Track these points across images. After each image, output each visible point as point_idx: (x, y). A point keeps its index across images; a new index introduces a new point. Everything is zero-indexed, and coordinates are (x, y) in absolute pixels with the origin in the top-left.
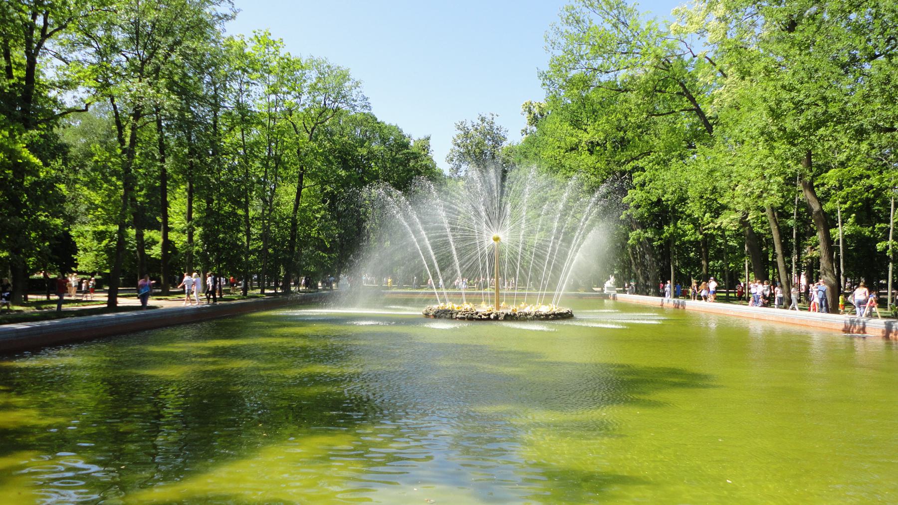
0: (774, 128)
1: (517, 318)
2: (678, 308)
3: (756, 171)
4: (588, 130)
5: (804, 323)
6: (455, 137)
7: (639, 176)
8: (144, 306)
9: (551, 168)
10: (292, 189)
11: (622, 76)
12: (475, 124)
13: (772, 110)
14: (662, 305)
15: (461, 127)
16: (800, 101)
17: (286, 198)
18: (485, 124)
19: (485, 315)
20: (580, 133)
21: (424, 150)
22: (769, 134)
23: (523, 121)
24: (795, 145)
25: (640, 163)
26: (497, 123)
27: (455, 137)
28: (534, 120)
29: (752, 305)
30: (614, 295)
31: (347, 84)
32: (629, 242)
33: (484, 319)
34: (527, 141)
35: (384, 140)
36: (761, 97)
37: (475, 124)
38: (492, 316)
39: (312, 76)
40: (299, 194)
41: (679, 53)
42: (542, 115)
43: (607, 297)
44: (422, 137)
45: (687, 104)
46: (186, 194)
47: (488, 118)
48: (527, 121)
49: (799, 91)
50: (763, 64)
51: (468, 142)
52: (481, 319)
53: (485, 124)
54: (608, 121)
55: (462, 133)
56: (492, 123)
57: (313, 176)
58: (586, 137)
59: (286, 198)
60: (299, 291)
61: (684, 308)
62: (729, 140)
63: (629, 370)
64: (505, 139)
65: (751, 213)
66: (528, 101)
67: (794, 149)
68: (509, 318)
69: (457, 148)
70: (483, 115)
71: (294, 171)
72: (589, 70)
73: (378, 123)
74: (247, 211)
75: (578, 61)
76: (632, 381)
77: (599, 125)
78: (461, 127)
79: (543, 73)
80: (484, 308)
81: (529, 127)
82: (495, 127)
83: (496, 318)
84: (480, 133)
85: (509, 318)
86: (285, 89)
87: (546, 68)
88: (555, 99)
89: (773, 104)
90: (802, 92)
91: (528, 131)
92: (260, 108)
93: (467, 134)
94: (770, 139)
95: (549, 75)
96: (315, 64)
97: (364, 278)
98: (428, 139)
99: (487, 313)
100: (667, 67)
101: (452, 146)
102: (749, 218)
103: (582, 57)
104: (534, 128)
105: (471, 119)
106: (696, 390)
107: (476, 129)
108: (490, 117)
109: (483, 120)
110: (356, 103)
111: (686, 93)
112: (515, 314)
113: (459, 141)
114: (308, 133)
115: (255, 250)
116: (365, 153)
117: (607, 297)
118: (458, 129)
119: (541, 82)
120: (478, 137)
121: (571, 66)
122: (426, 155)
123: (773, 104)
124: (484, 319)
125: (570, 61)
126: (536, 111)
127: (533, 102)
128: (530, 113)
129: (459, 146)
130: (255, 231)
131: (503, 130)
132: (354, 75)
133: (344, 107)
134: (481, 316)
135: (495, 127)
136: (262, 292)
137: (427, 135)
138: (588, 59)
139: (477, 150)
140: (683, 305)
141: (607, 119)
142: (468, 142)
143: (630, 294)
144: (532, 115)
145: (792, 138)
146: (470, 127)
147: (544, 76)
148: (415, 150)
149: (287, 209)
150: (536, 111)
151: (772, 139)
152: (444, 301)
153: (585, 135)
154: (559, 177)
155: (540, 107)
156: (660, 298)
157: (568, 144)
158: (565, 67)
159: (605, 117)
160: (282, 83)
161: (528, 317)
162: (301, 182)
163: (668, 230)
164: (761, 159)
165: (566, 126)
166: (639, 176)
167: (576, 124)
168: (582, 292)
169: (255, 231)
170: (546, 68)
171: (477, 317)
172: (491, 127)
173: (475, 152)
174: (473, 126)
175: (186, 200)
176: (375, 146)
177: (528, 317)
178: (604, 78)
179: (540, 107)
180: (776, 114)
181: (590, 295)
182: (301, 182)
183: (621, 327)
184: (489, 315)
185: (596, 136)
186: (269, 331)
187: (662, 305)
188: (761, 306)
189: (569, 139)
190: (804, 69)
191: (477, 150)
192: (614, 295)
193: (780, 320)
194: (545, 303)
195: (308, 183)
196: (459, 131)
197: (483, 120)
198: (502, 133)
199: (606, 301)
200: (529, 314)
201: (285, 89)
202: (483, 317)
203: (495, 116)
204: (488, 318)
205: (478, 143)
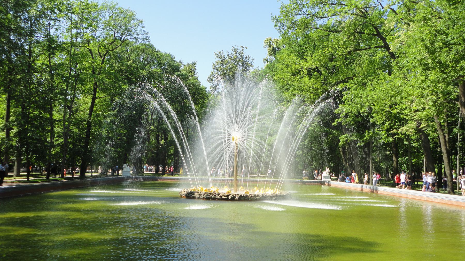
0: (430, 61)
1: (248, 199)
2: (373, 192)
3: (418, 91)
4: (308, 59)
5: (459, 204)
6: (215, 63)
7: (347, 94)
8: (28, 181)
9: (283, 87)
10: (89, 99)
11: (332, 21)
12: (230, 54)
13: (426, 47)
14: (362, 190)
15: (220, 55)
16: (448, 41)
17: (84, 106)
18: (237, 54)
19: (225, 196)
20: (302, 62)
21: (191, 72)
22: (426, 64)
23: (265, 52)
24: (444, 73)
25: (348, 85)
26: (246, 53)
27: (215, 63)
28: (273, 52)
29: (425, 191)
30: (329, 182)
31: (132, 22)
32: (340, 143)
33: (224, 199)
34: (268, 67)
35: (160, 64)
36: (420, 38)
37: (230, 54)
38: (230, 197)
39: (106, 15)
40: (93, 104)
41: (373, 5)
42: (279, 48)
43: (322, 183)
44: (190, 63)
45: (380, 42)
46: (6, 101)
47: (240, 49)
48: (268, 53)
49: (447, 35)
50: (422, 15)
51: (224, 67)
52: (222, 199)
53: (237, 54)
54: (322, 53)
55: (220, 60)
56: (243, 53)
57: (103, 90)
58: (306, 65)
59: (84, 106)
60: (92, 176)
61: (377, 193)
62: (403, 69)
63: (318, 239)
64: (252, 65)
65: (423, 123)
66: (268, 38)
67: (444, 76)
68: (243, 198)
69: (216, 71)
70: (236, 48)
71: (89, 86)
72: (309, 16)
73: (156, 52)
74: (51, 115)
75: (300, 9)
76: (322, 247)
77: (316, 56)
78: (220, 55)
79: (276, 17)
80: (224, 191)
81: (269, 57)
82: (245, 56)
83: (233, 199)
84: (234, 60)
85: (242, 198)
86: (84, 25)
87: (277, 13)
88: (285, 36)
89: (428, 43)
90: (450, 35)
91: (269, 60)
92: (66, 39)
93: (223, 62)
94: (426, 68)
95: (280, 19)
96: (106, 7)
97: (145, 167)
98: (195, 64)
99: (226, 194)
100: (365, 16)
101: (212, 70)
102: (421, 126)
103: (304, 5)
104: (273, 57)
105: (227, 50)
106: (367, 254)
107: (231, 58)
108: (241, 49)
109: (236, 51)
110: (138, 37)
111: (379, 35)
112: (247, 196)
113: (218, 66)
114: (101, 57)
115: (58, 145)
116: (145, 74)
117: (322, 183)
118: (217, 57)
119: (274, 24)
120: (232, 63)
121: (296, 12)
122: (192, 76)
123: (428, 43)
124: (224, 199)
125: (295, 8)
126: (274, 45)
127: (273, 39)
128: (270, 47)
129: (217, 70)
130: (58, 129)
131: (251, 58)
132: (138, 16)
133: (131, 40)
134: (221, 197)
135: (245, 56)
136: (62, 177)
137: (194, 61)
138: (308, 8)
139: (231, 73)
140: (377, 190)
141: (322, 52)
142: (224, 67)
143: (340, 181)
144: (271, 49)
145: (443, 67)
146: (226, 56)
147: (275, 19)
148: (184, 72)
149: (83, 114)
150: (274, 45)
151: (428, 69)
152: (194, 185)
153: (306, 63)
154: (287, 95)
155: (277, 43)
156: (361, 185)
157: (293, 69)
158: (292, 13)
159: (320, 50)
160: (82, 21)
161: (257, 198)
162: (95, 95)
163: (367, 135)
164: (420, 84)
165: (293, 57)
166: (347, 94)
167: (301, 55)
168: (305, 180)
169: (58, 129)
170: (277, 13)
171: (218, 197)
172: (242, 56)
173: (229, 75)
174: (228, 55)
175: (5, 106)
176: (154, 69)
177: (257, 198)
178: (319, 22)
179: (277, 43)
180: (431, 51)
181: (311, 182)
182: (95, 95)
183: (283, 210)
184: (228, 196)
185: (313, 65)
186: (60, 206)
187: (362, 190)
188: (431, 192)
189: (293, 66)
190: (450, 19)
191: (231, 73)
192: (329, 182)
193: (443, 202)
194: (272, 188)
195: (101, 95)
196: (218, 59)
197: (236, 51)
198: (250, 61)
199: (322, 186)
200: (258, 196)
201: (84, 25)
202: (223, 197)
203: (245, 49)
204: (227, 199)
205: (232, 68)
